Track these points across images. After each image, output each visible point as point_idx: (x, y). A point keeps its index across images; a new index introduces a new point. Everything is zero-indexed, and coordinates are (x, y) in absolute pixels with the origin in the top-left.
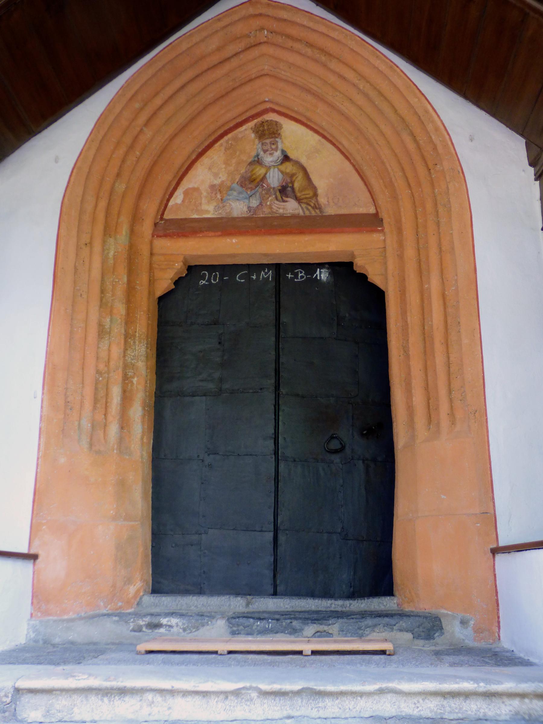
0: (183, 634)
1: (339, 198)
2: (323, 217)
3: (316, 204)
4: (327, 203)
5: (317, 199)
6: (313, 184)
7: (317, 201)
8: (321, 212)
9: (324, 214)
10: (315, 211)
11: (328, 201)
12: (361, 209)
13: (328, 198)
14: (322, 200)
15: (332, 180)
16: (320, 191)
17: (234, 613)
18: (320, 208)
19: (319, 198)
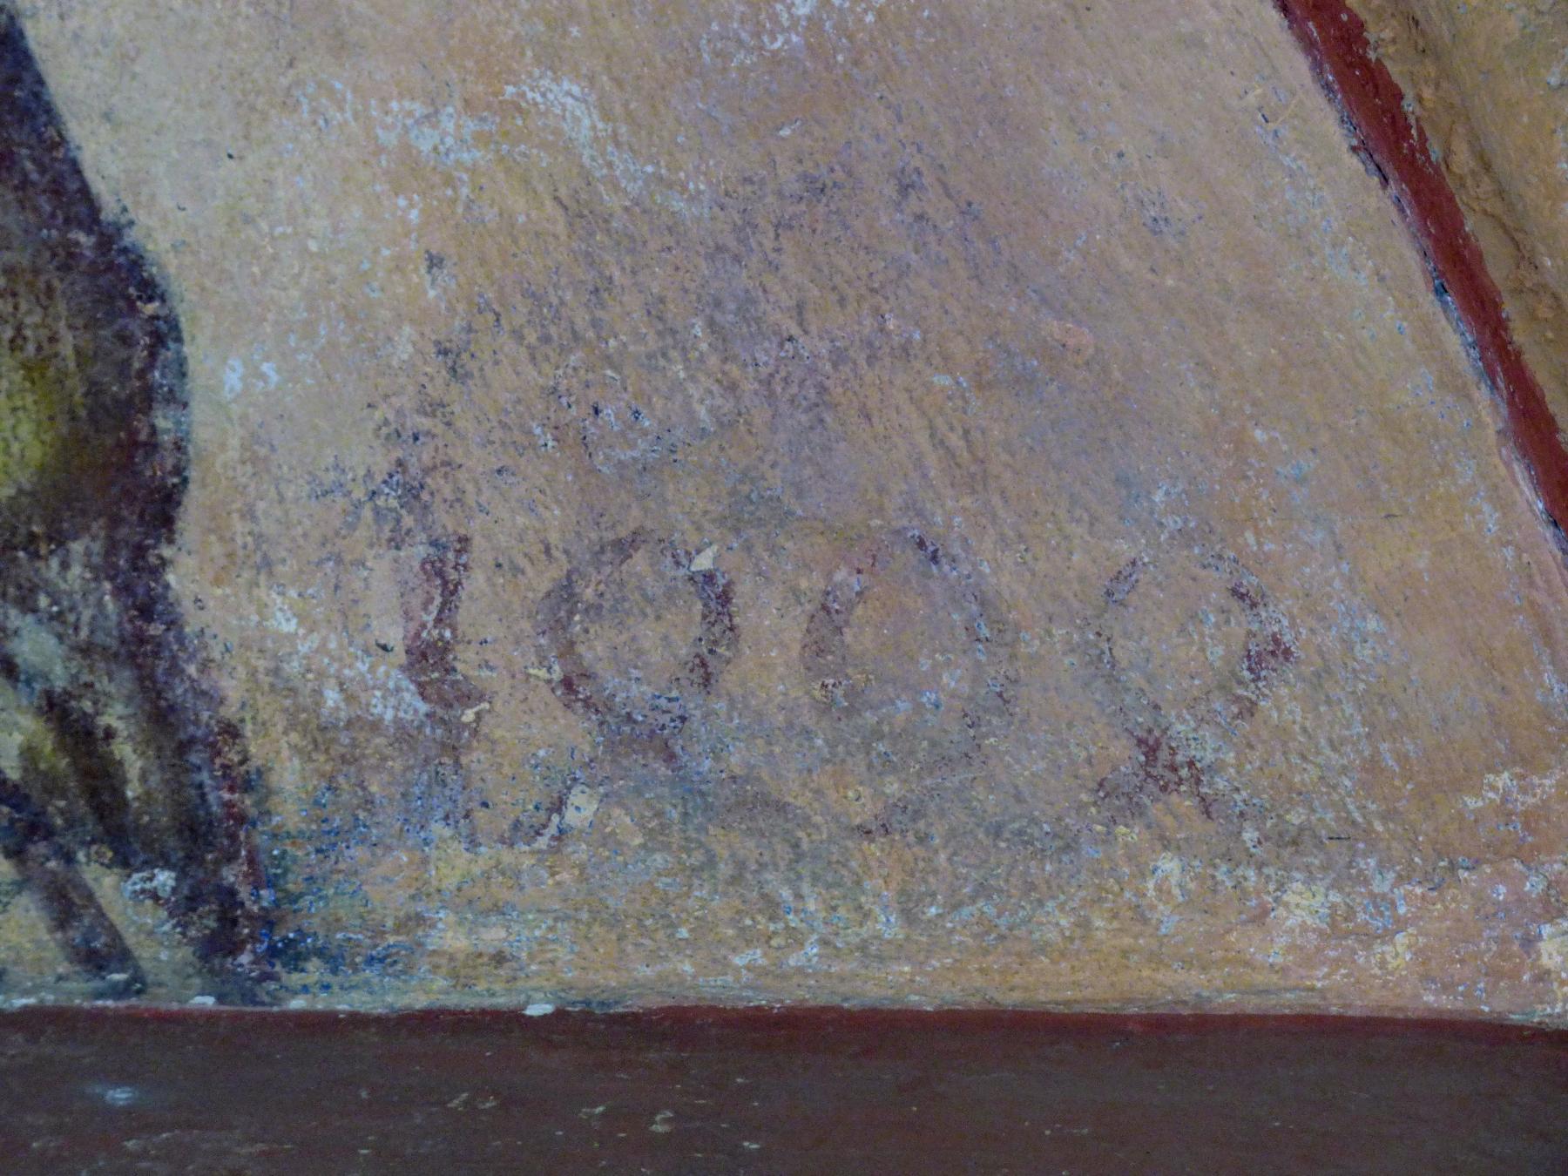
0: (402, 554)
1: (717, 596)
2: (256, 1049)
3: (116, 716)
4: (396, 700)
5: (148, 604)
6: (70, 195)
7: (146, 638)
8: (224, 929)
9: (304, 993)
10: (66, 903)
11: (428, 658)
12: (1304, 905)
13: (443, 576)
14: (279, 618)
15: (566, 101)
16: (232, 387)
17: (79, 148)
18: (204, 837)
19: (187, 573)
